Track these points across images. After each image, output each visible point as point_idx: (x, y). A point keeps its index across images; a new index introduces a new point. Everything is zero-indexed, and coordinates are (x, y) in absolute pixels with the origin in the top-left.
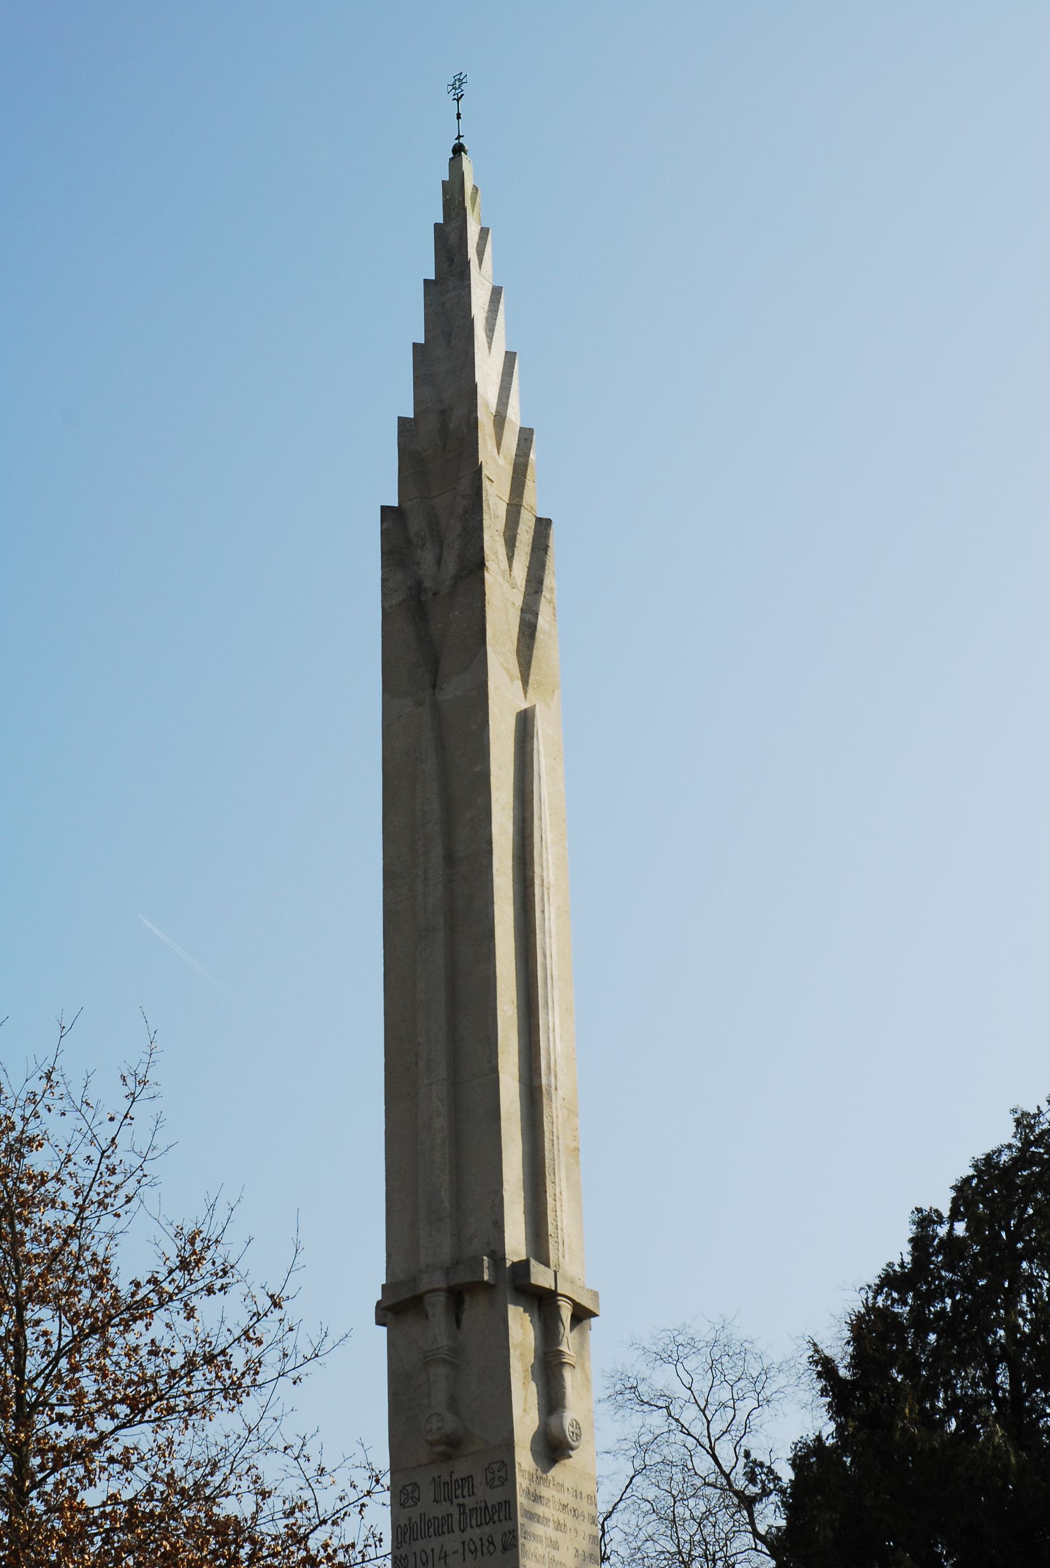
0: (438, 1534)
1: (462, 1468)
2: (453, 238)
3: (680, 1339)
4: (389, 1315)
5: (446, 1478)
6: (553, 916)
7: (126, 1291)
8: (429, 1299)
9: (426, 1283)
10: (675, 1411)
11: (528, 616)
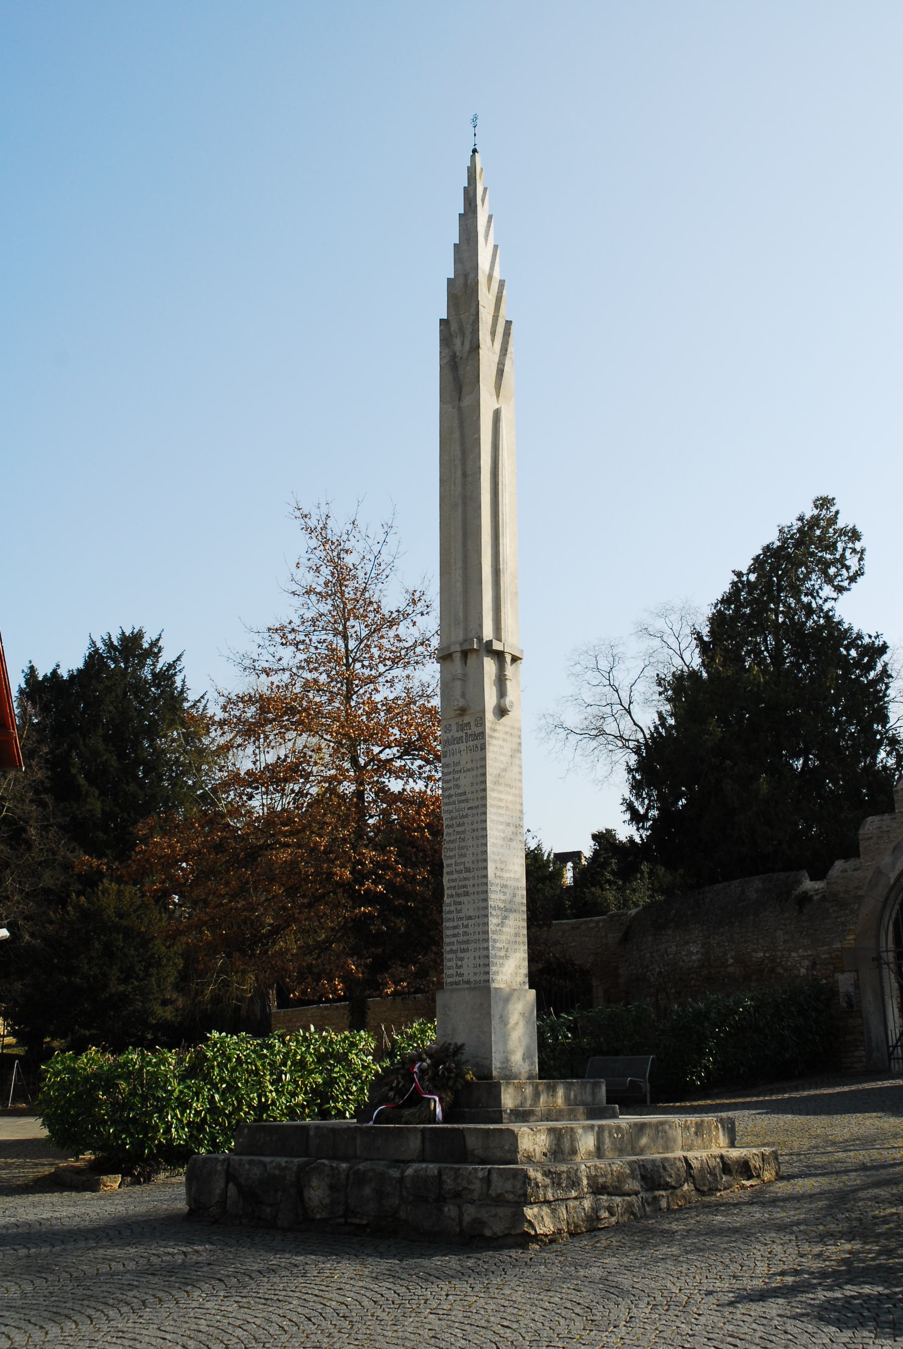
0: (457, 743)
1: (467, 719)
2: (471, 193)
3: (667, 607)
4: (441, 660)
5: (461, 723)
6: (507, 497)
7: (387, 615)
8: (454, 655)
9: (453, 649)
10: (665, 639)
11: (500, 366)
